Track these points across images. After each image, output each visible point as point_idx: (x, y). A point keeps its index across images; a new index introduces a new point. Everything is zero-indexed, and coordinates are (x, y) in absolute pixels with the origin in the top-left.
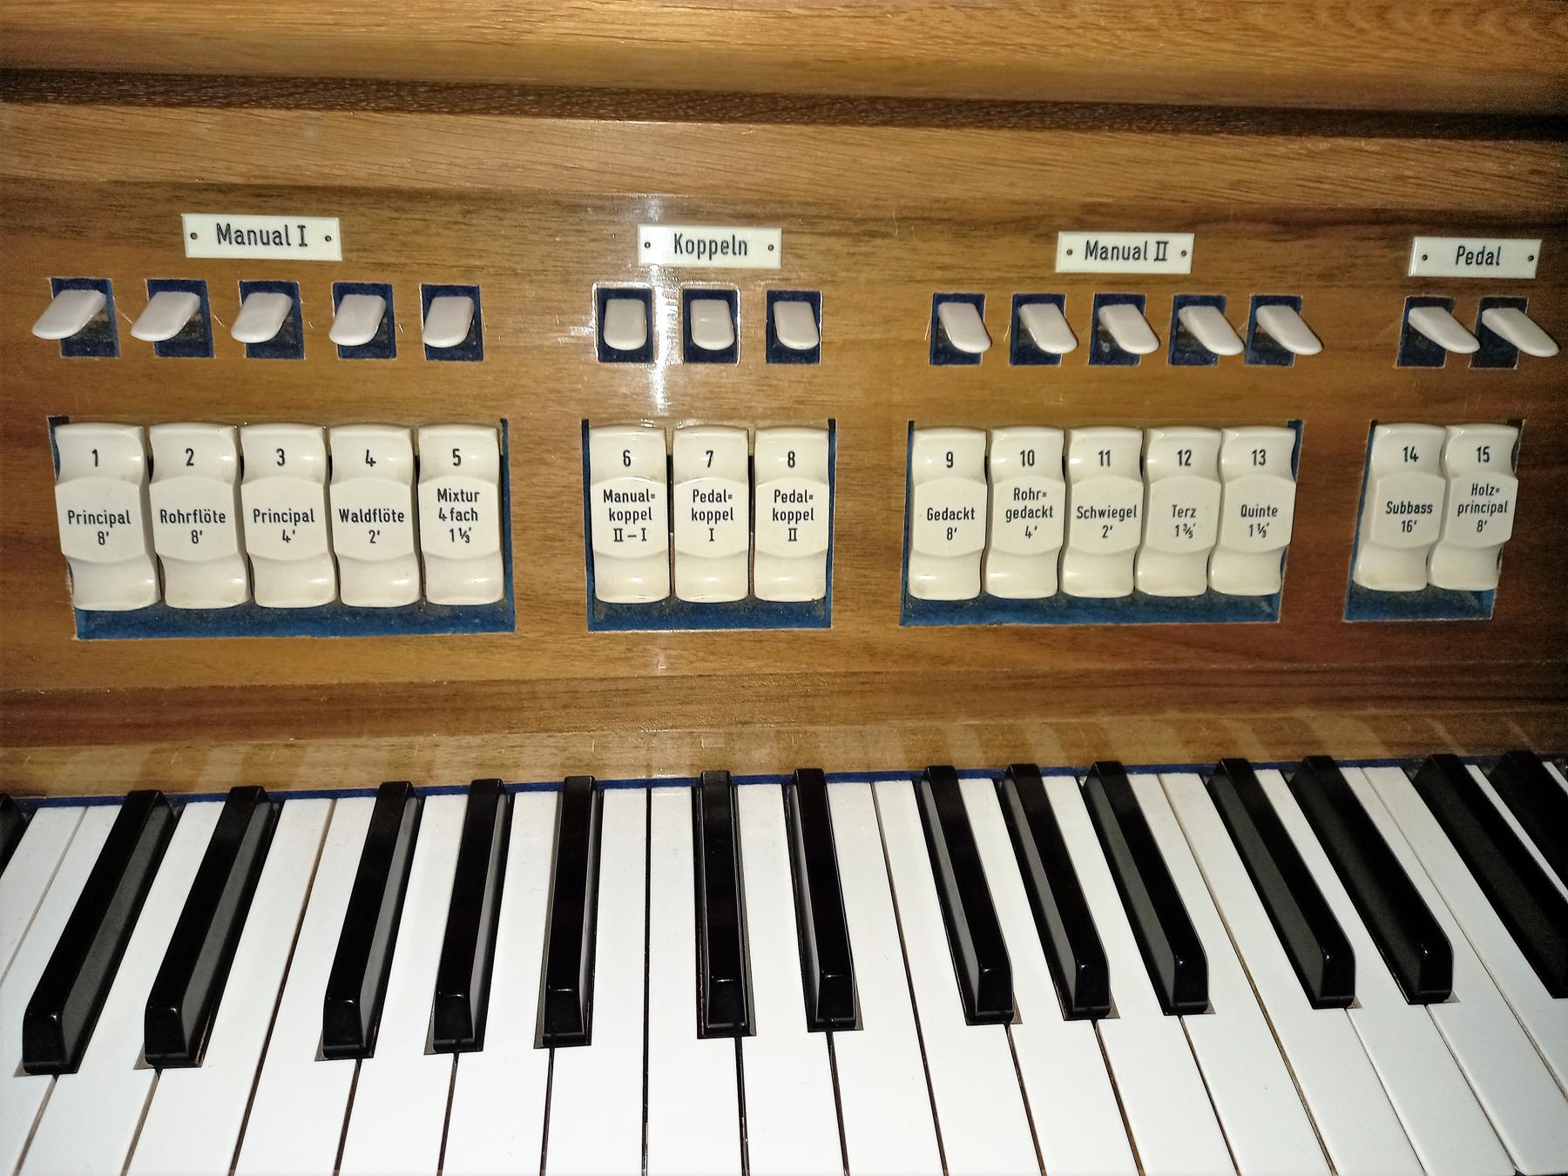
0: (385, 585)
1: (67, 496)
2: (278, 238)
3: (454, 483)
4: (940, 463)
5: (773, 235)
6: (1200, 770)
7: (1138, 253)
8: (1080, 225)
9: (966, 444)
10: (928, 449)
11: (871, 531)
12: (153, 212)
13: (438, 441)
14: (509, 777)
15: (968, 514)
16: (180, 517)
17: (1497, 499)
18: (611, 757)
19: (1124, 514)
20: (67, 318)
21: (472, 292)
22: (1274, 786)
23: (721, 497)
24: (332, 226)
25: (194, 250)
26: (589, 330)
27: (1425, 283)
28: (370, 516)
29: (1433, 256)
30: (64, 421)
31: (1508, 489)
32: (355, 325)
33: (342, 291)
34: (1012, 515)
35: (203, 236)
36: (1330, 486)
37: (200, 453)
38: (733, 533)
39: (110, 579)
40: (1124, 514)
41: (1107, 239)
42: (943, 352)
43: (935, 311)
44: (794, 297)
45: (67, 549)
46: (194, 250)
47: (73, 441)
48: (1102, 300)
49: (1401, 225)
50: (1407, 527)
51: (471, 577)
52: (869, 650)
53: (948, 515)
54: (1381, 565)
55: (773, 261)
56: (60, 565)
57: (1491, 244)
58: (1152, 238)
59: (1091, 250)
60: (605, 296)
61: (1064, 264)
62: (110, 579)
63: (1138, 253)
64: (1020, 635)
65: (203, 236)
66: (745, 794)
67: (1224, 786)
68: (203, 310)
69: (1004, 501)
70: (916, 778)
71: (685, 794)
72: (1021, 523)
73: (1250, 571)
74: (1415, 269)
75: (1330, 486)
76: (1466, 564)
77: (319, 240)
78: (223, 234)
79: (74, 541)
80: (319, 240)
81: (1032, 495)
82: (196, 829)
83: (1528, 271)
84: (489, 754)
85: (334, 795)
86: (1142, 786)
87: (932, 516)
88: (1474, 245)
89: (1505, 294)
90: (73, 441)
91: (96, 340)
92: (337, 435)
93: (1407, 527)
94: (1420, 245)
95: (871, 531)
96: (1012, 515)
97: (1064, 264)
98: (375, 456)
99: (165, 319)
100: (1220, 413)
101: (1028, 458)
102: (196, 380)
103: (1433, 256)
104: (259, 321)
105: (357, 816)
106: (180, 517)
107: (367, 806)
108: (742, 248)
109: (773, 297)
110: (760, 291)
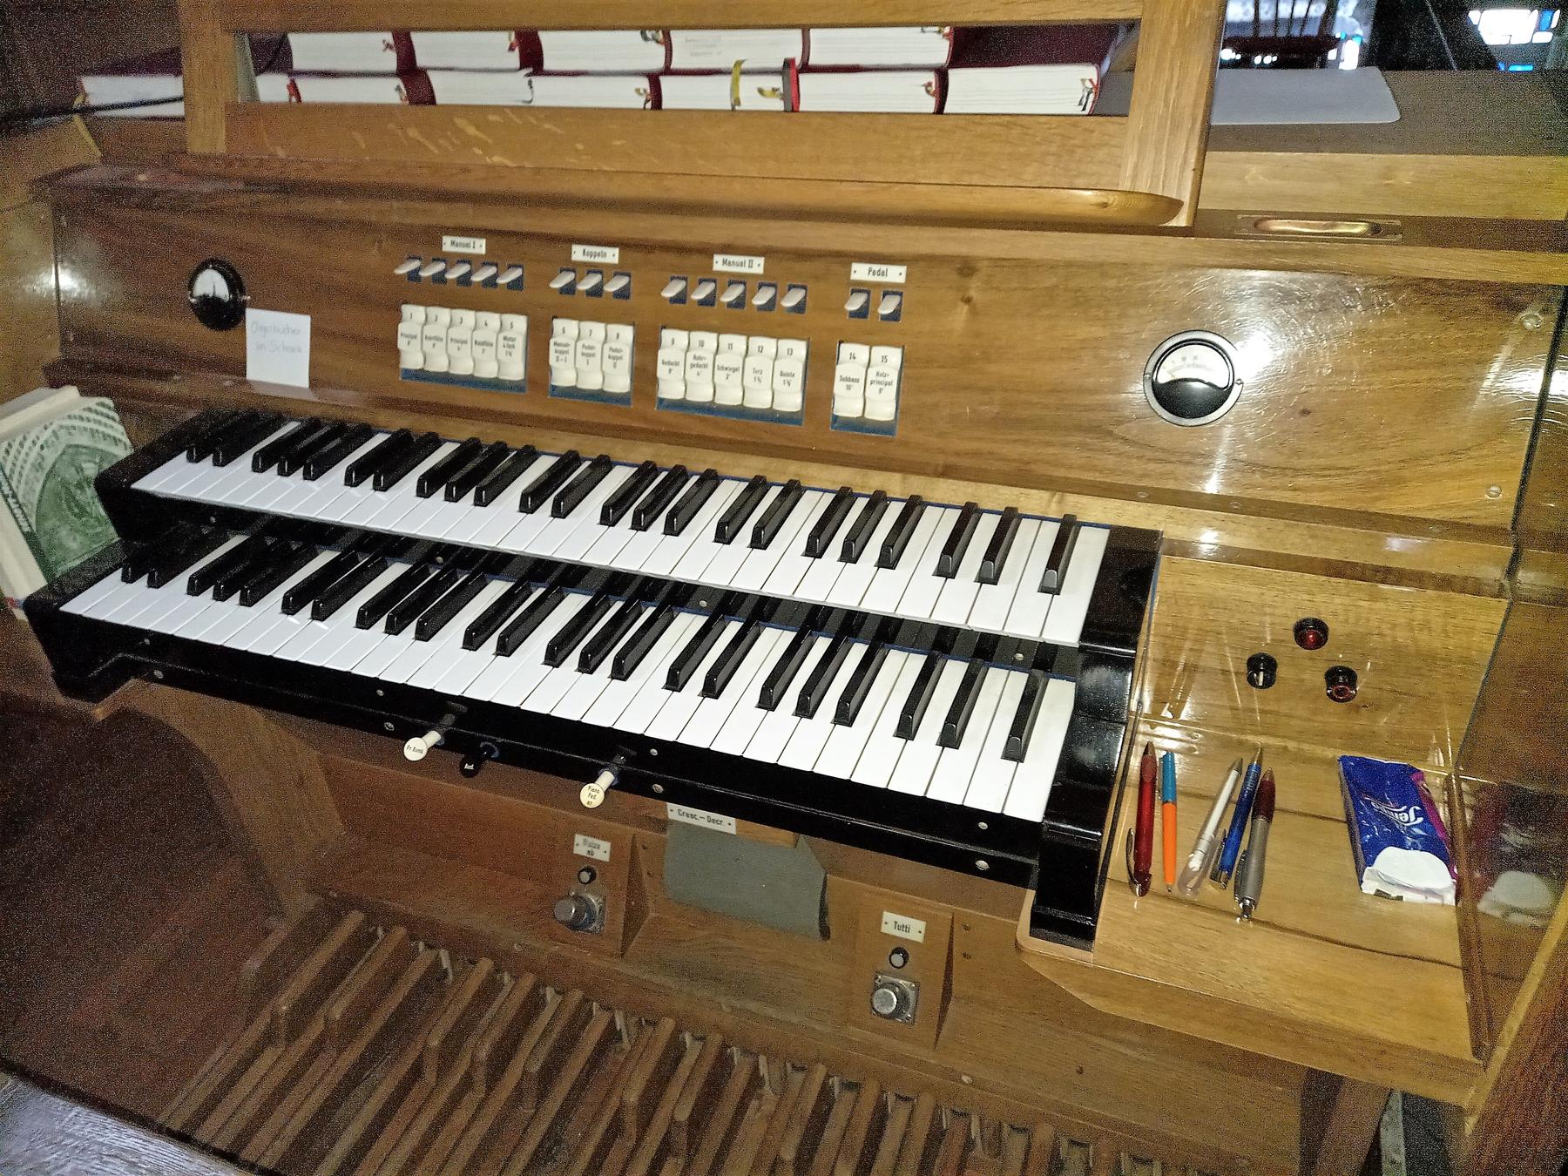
2: (467, 245)
3: (509, 334)
7: (742, 264)
14: (982, 506)
17: (888, 379)
20: (671, 292)
23: (591, 348)
30: (664, 327)
32: (761, 298)
36: (820, 369)
39: (412, 359)
40: (735, 370)
45: (659, 374)
50: (849, 388)
53: (669, 363)
54: (847, 404)
56: (397, 352)
57: (884, 267)
58: (747, 259)
63: (742, 264)
64: (702, 420)
68: (867, 302)
69: (690, 360)
71: (1107, 532)
72: (696, 370)
73: (791, 401)
74: (854, 277)
75: (820, 369)
76: (883, 408)
79: (402, 343)
81: (700, 358)
83: (902, 280)
87: (842, 379)
88: (876, 267)
90: (407, 309)
91: (681, 299)
93: (849, 388)
94: (855, 266)
99: (700, 294)
100: (778, 332)
102: (441, 294)
104: (730, 295)
105: (1052, 530)
107: (1057, 526)
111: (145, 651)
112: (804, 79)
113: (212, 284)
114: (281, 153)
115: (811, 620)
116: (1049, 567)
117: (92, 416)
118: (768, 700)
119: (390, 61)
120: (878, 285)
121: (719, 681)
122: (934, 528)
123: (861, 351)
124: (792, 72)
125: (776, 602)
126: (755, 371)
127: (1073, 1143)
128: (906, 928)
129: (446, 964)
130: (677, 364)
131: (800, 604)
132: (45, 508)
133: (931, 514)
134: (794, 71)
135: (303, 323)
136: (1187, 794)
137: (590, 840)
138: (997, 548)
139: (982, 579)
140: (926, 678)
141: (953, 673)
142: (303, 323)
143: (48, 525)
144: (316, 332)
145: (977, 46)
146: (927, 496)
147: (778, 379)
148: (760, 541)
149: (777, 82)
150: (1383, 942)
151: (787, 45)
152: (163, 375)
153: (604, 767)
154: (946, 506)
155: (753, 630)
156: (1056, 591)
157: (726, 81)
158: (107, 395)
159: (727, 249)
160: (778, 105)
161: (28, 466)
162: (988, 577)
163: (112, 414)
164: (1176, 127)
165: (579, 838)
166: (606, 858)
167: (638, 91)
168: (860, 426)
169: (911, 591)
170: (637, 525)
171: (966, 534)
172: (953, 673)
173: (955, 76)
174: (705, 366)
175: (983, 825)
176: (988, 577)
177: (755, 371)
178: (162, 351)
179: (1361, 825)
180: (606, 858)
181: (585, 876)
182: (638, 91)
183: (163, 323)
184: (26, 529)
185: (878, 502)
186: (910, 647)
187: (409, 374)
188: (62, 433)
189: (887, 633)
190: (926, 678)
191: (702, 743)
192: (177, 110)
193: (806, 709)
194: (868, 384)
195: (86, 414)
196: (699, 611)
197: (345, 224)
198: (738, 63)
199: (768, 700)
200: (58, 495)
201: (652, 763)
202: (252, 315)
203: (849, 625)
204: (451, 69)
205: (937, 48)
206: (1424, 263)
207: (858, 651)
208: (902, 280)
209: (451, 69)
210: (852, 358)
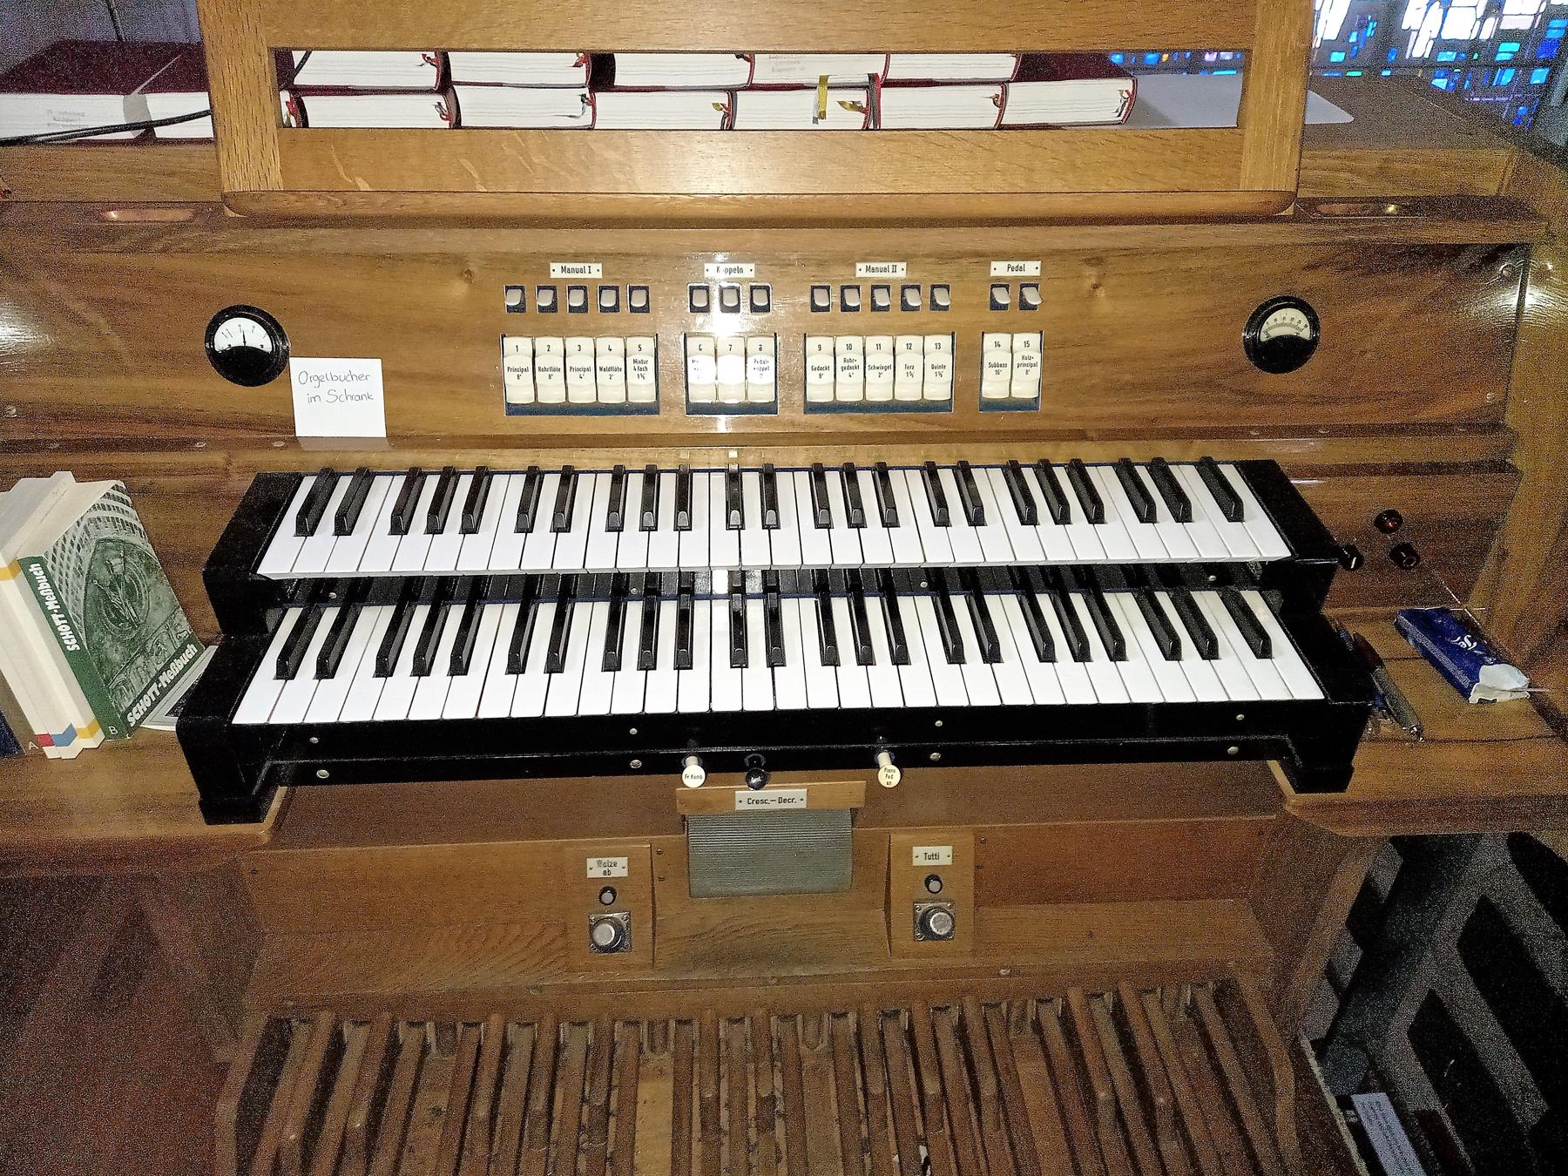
0: (612, 394)
1: (508, 362)
4: (819, 350)
5: (752, 266)
6: (1113, 465)
8: (863, 260)
9: (1004, 338)
10: (989, 340)
11: (791, 377)
12: (541, 262)
13: (633, 343)
15: (827, 368)
16: (546, 369)
18: (695, 458)
19: (886, 368)
20: (513, 299)
21: (522, 288)
22: (1142, 472)
24: (599, 266)
25: (553, 275)
26: (807, 299)
27: (998, 279)
28: (610, 369)
29: (999, 269)
31: (1037, 358)
33: (602, 289)
34: (843, 369)
35: (556, 271)
36: (968, 361)
37: (548, 348)
38: (828, 375)
40: (886, 368)
41: (570, 266)
42: (995, 306)
43: (932, 295)
44: (912, 287)
46: (553, 275)
47: (510, 343)
48: (1022, 286)
49: (985, 257)
50: (998, 372)
51: (643, 392)
52: (793, 424)
53: (819, 368)
54: (993, 387)
55: (752, 275)
57: (1021, 264)
59: (868, 269)
60: (692, 289)
61: (859, 274)
62: (519, 391)
63: (885, 270)
65: (556, 271)
66: (860, 474)
67: (1075, 473)
69: (840, 363)
70: (921, 469)
73: (939, 390)
75: (968, 361)
76: (1026, 386)
77: (595, 271)
78: (563, 269)
80: (595, 271)
82: (432, 483)
83: (1037, 273)
84: (650, 456)
85: (596, 472)
86: (1091, 471)
87: (991, 366)
88: (1014, 264)
89: (1026, 284)
90: (510, 343)
92: (599, 340)
93: (998, 372)
94: (994, 264)
95: (791, 377)
96: (843, 369)
97: (859, 274)
98: (610, 349)
101: (849, 347)
103: (999, 269)
106: (546, 369)
107: (400, 481)
108: (741, 271)
109: (904, 288)
110: (870, 284)
111: (312, 751)
112: (886, 93)
113: (240, 333)
114: (364, 186)
115: (404, 592)
116: (643, 512)
117: (112, 503)
118: (384, 668)
119: (430, 77)
120: (1017, 279)
121: (331, 661)
122: (505, 493)
123: (524, 344)
124: (876, 87)
125: (369, 581)
126: (907, 367)
127: (679, 1022)
128: (936, 856)
129: (431, 1038)
130: (827, 368)
131: (464, 578)
132: (91, 621)
133: (499, 482)
134: (875, 84)
135: (373, 367)
136: (1389, 660)
137: (605, 860)
138: (683, 501)
139: (556, 530)
140: (524, 623)
141: (546, 614)
142: (373, 367)
143: (95, 637)
144: (387, 376)
145: (1033, 68)
146: (578, 466)
147: (930, 373)
148: (344, 527)
149: (861, 97)
150: (1489, 730)
151: (875, 64)
152: (184, 445)
153: (685, 756)
154: (393, 474)
155: (407, 612)
156: (620, 530)
157: (809, 97)
158: (117, 478)
159: (562, 257)
160: (857, 120)
161: (71, 573)
162: (469, 528)
163: (125, 497)
164: (1283, 134)
165: (591, 862)
166: (625, 873)
167: (716, 105)
168: (1010, 405)
169: (496, 549)
170: (649, 528)
171: (480, 499)
172: (546, 614)
173: (1015, 89)
174: (857, 367)
175: (315, 740)
176: (469, 528)
177: (907, 367)
178: (172, 419)
179: (1457, 653)
180: (625, 873)
181: (608, 897)
182: (716, 105)
183: (166, 384)
184: (73, 646)
185: (449, 476)
186: (502, 599)
187: (515, 410)
188: (91, 528)
189: (476, 591)
190: (524, 623)
191: (432, 714)
192: (203, 129)
193: (422, 668)
194: (1014, 368)
195: (107, 502)
196: (333, 604)
197: (418, 258)
198: (823, 80)
199: (384, 668)
200: (97, 603)
201: (312, 751)
202: (295, 364)
203: (441, 591)
204: (501, 85)
205: (1005, 65)
206: (1447, 234)
207: (456, 614)
208: (1037, 273)
209: (501, 85)
210: (995, 347)
